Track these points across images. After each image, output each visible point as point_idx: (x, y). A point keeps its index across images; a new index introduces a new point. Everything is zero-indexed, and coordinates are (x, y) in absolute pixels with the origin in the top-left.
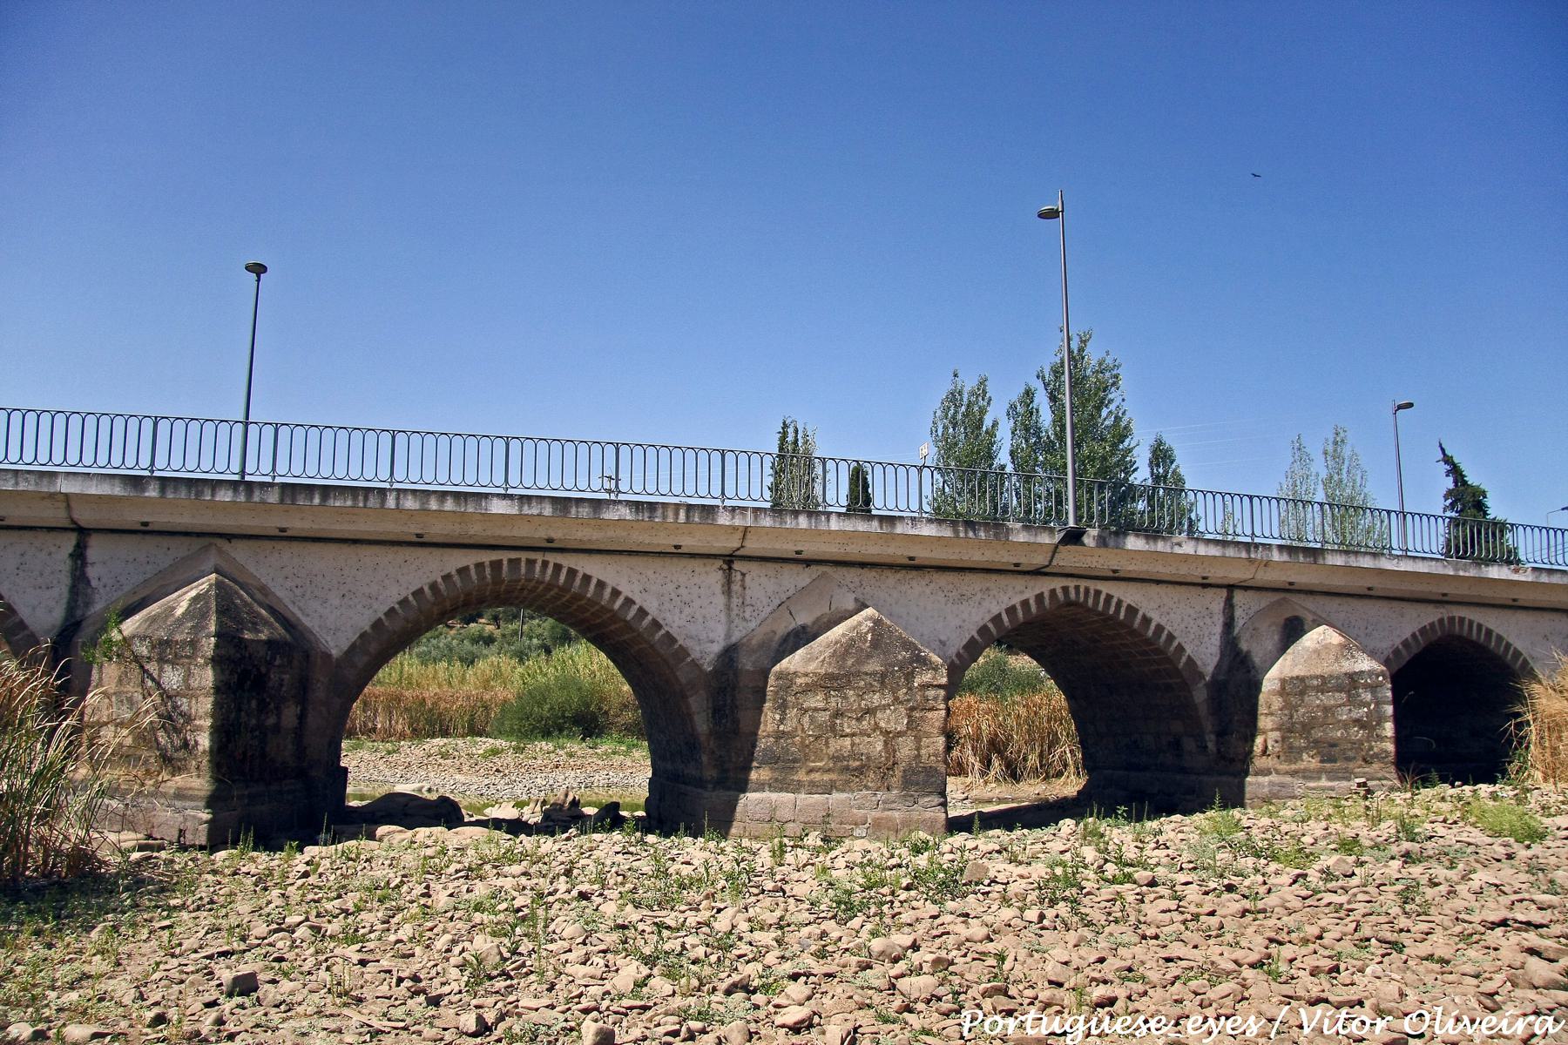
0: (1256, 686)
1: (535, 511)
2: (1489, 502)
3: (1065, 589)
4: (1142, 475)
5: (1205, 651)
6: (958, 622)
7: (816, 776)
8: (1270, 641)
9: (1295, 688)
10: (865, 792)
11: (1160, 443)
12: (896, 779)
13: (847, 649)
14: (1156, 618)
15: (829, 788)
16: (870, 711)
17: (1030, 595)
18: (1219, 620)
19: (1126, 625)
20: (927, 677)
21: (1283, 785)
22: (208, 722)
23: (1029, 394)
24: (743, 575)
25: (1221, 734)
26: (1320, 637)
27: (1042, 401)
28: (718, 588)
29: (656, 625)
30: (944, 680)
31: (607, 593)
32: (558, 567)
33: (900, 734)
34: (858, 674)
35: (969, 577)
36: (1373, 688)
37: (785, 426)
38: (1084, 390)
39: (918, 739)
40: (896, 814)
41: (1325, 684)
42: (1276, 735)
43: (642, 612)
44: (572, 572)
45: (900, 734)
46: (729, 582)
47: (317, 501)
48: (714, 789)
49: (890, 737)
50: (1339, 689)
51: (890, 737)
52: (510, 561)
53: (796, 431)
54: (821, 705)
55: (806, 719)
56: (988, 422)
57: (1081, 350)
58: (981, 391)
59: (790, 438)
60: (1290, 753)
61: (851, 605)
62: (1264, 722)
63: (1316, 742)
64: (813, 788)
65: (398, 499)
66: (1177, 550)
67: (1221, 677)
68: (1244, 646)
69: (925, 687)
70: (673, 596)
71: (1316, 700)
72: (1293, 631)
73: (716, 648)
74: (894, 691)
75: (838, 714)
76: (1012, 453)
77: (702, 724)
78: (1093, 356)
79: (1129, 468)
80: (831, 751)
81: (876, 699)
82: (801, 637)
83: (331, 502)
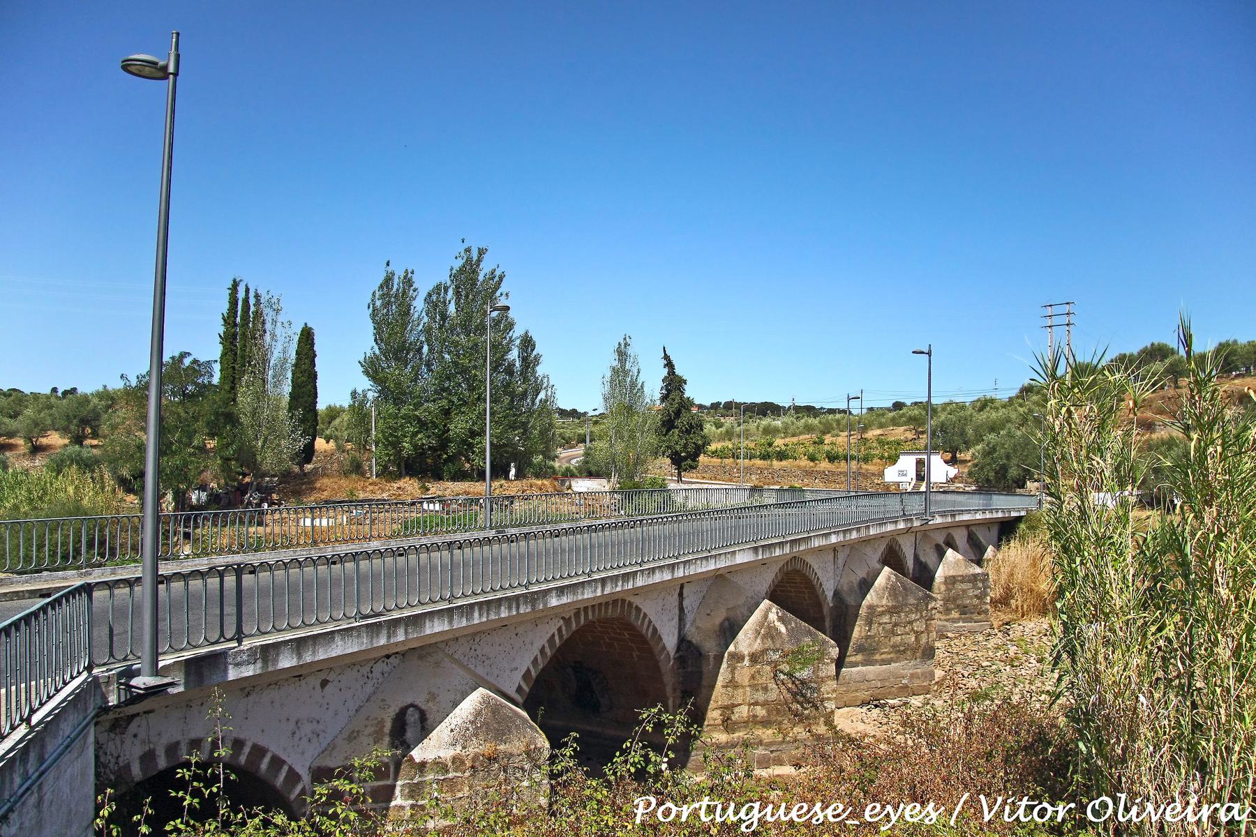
0: (932, 579)
9: (951, 581)
15: (888, 662)
16: (911, 623)
34: (906, 605)
37: (235, 285)
38: (473, 285)
41: (964, 579)
53: (247, 291)
57: (479, 261)
58: (408, 282)
64: (884, 662)
71: (959, 586)
72: (941, 554)
75: (896, 625)
81: (913, 616)
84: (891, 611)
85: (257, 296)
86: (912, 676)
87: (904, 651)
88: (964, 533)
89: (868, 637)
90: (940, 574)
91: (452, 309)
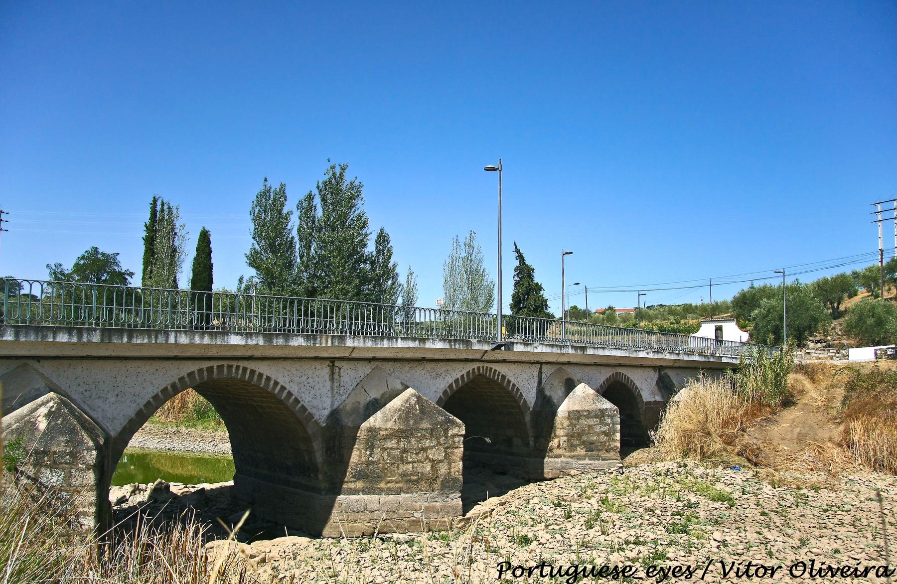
0: (554, 413)
1: (254, 342)
2: (535, 274)
3: (478, 368)
4: (371, 248)
5: (530, 396)
6: (435, 389)
7: (391, 485)
8: (560, 392)
9: (575, 416)
10: (419, 493)
11: (382, 231)
12: (437, 485)
13: (406, 413)
14: (513, 381)
15: (398, 492)
16: (424, 449)
17: (464, 372)
18: (536, 379)
19: (500, 385)
20: (455, 431)
21: (567, 463)
22: (93, 509)
23: (310, 198)
24: (340, 369)
25: (537, 438)
26: (581, 389)
27: (317, 201)
28: (327, 378)
29: (297, 401)
30: (464, 432)
31: (272, 384)
32: (245, 369)
33: (441, 461)
34: (417, 430)
35: (441, 364)
36: (612, 417)
37: (155, 201)
38: (338, 195)
39: (450, 464)
40: (438, 504)
41: (589, 414)
42: (565, 438)
43: (290, 394)
44: (253, 372)
45: (441, 461)
46: (333, 373)
47: (125, 340)
48: (326, 494)
49: (434, 463)
50: (596, 417)
51: (434, 463)
52: (218, 366)
54: (395, 446)
55: (386, 454)
56: (285, 211)
58: (282, 193)
59: (159, 208)
60: (572, 447)
61: (400, 387)
62: (560, 432)
63: (584, 442)
64: (390, 492)
65: (176, 337)
66: (536, 350)
67: (538, 409)
68: (548, 393)
69: (454, 436)
70: (306, 383)
71: (584, 422)
72: (570, 386)
73: (327, 412)
74: (438, 439)
75: (405, 451)
76: (299, 231)
77: (319, 457)
78: (348, 178)
79: (363, 244)
80: (400, 471)
81: (427, 443)
82: (375, 406)
83: (134, 341)
84: (397, 435)
85: (169, 208)
86: (428, 510)
87: (417, 481)
88: (654, 376)
89: (369, 463)
90: (563, 410)
91: (320, 213)
